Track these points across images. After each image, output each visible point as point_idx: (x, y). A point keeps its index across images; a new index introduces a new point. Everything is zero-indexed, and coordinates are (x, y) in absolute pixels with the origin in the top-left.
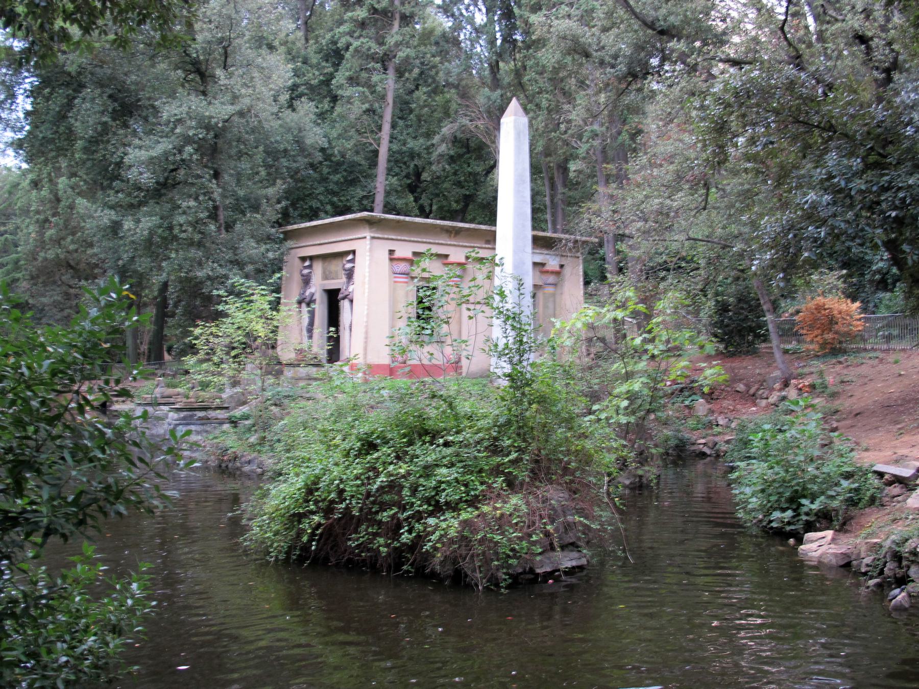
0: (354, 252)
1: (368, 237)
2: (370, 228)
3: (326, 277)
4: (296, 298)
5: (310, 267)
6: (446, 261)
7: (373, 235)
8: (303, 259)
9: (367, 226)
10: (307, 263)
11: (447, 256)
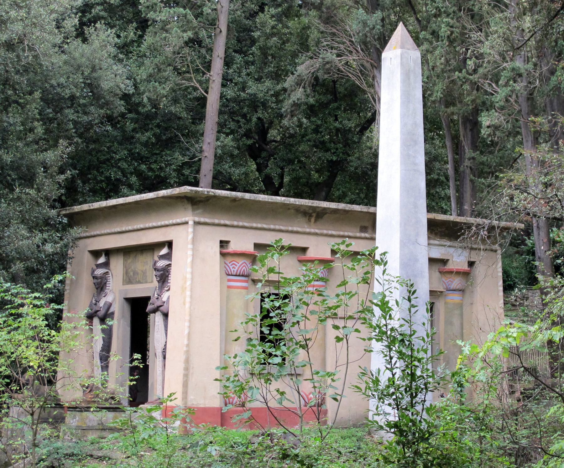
0: (170, 244)
1: (191, 223)
2: (193, 210)
3: (129, 280)
4: (84, 311)
5: (106, 265)
6: (302, 257)
7: (197, 219)
8: (96, 254)
9: (189, 207)
10: (102, 260)
11: (304, 250)
